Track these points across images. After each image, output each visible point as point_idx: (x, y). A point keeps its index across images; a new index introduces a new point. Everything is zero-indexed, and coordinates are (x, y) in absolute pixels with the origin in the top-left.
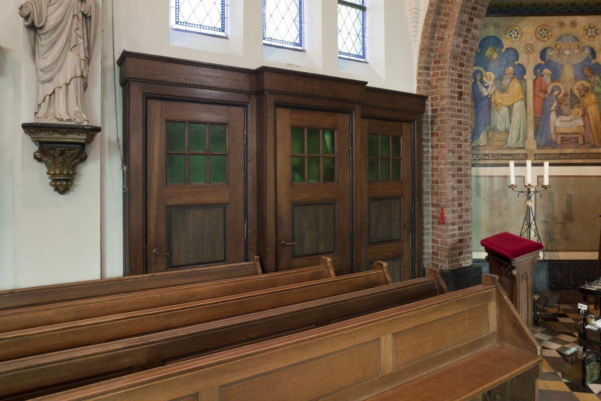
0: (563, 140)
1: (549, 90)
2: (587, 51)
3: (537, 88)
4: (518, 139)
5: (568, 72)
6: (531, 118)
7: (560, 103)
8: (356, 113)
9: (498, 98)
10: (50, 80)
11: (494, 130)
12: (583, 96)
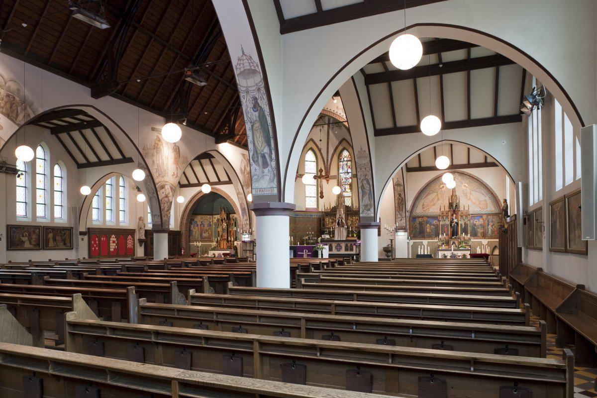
5: (206, 225)
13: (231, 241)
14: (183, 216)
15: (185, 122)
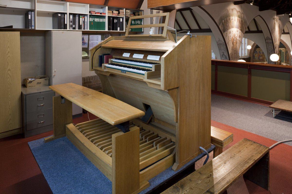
15: (253, 3)
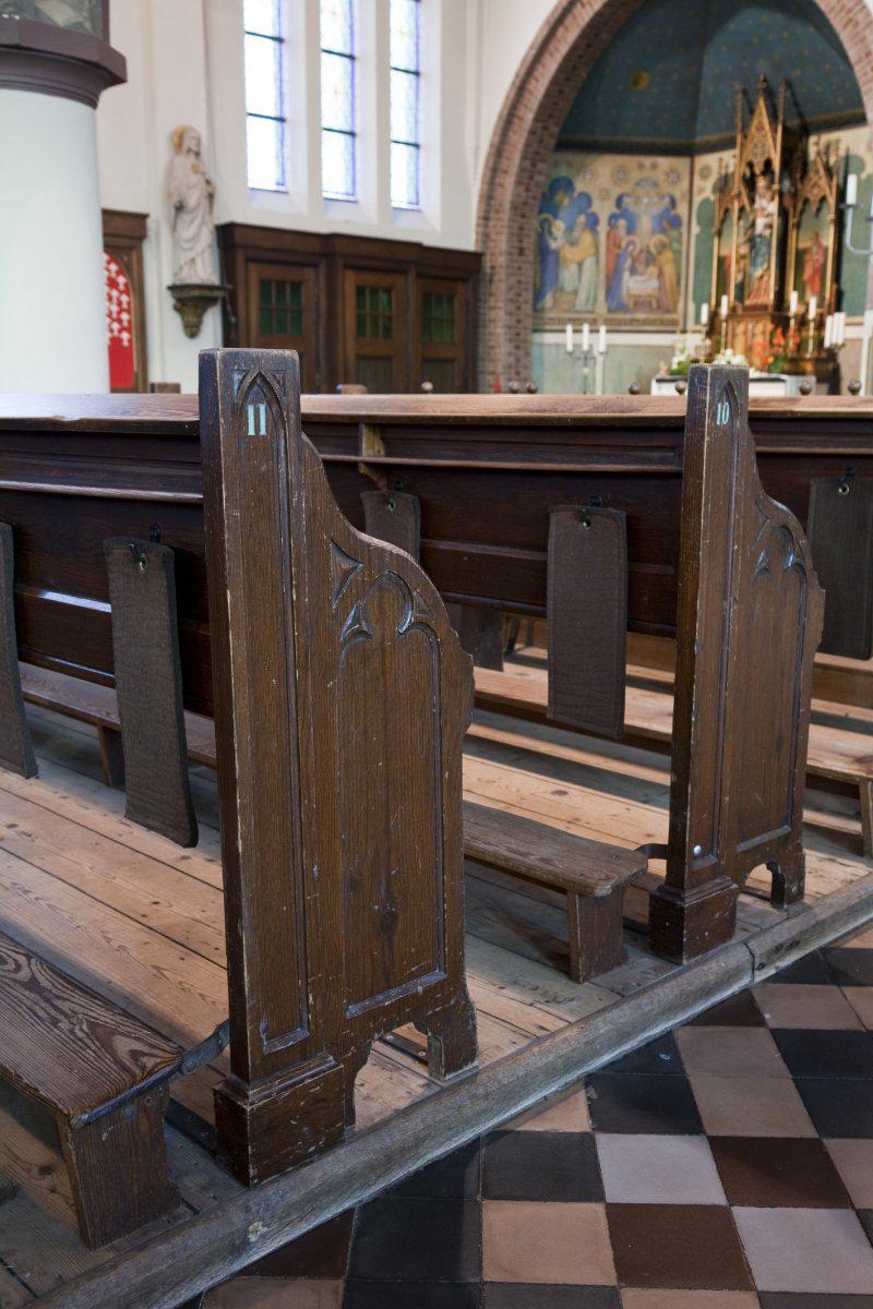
0: (636, 304)
1: (623, 245)
2: (667, 201)
3: (611, 243)
4: (588, 300)
5: (645, 224)
6: (602, 276)
7: (634, 261)
8: (413, 272)
9: (568, 253)
10: (191, 249)
11: (562, 290)
12: (660, 253)
13: (803, 321)
14: (499, 151)
